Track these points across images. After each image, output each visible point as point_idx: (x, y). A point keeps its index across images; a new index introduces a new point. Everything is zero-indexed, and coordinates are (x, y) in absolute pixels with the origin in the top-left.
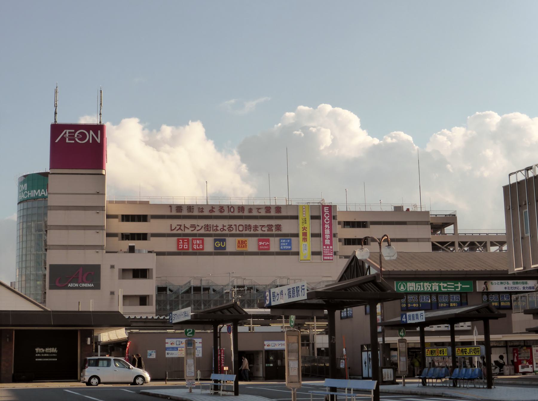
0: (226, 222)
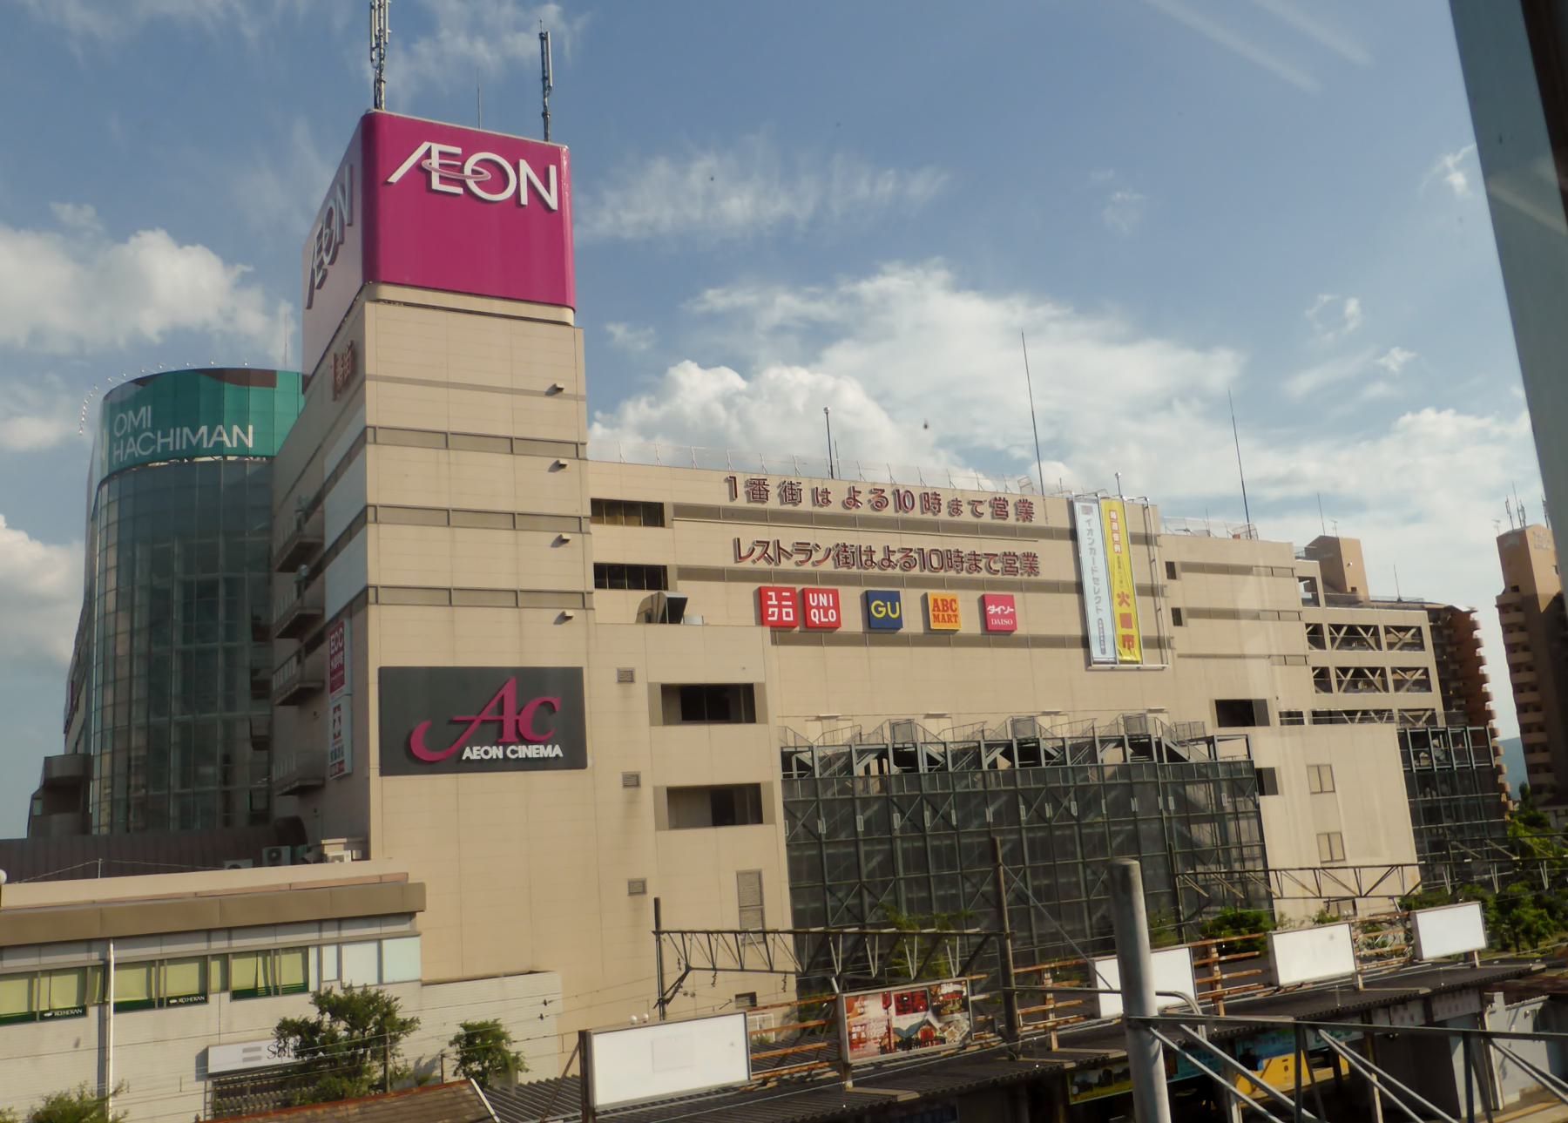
0: (897, 541)
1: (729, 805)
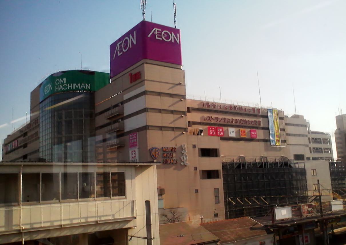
1: (210, 174)
